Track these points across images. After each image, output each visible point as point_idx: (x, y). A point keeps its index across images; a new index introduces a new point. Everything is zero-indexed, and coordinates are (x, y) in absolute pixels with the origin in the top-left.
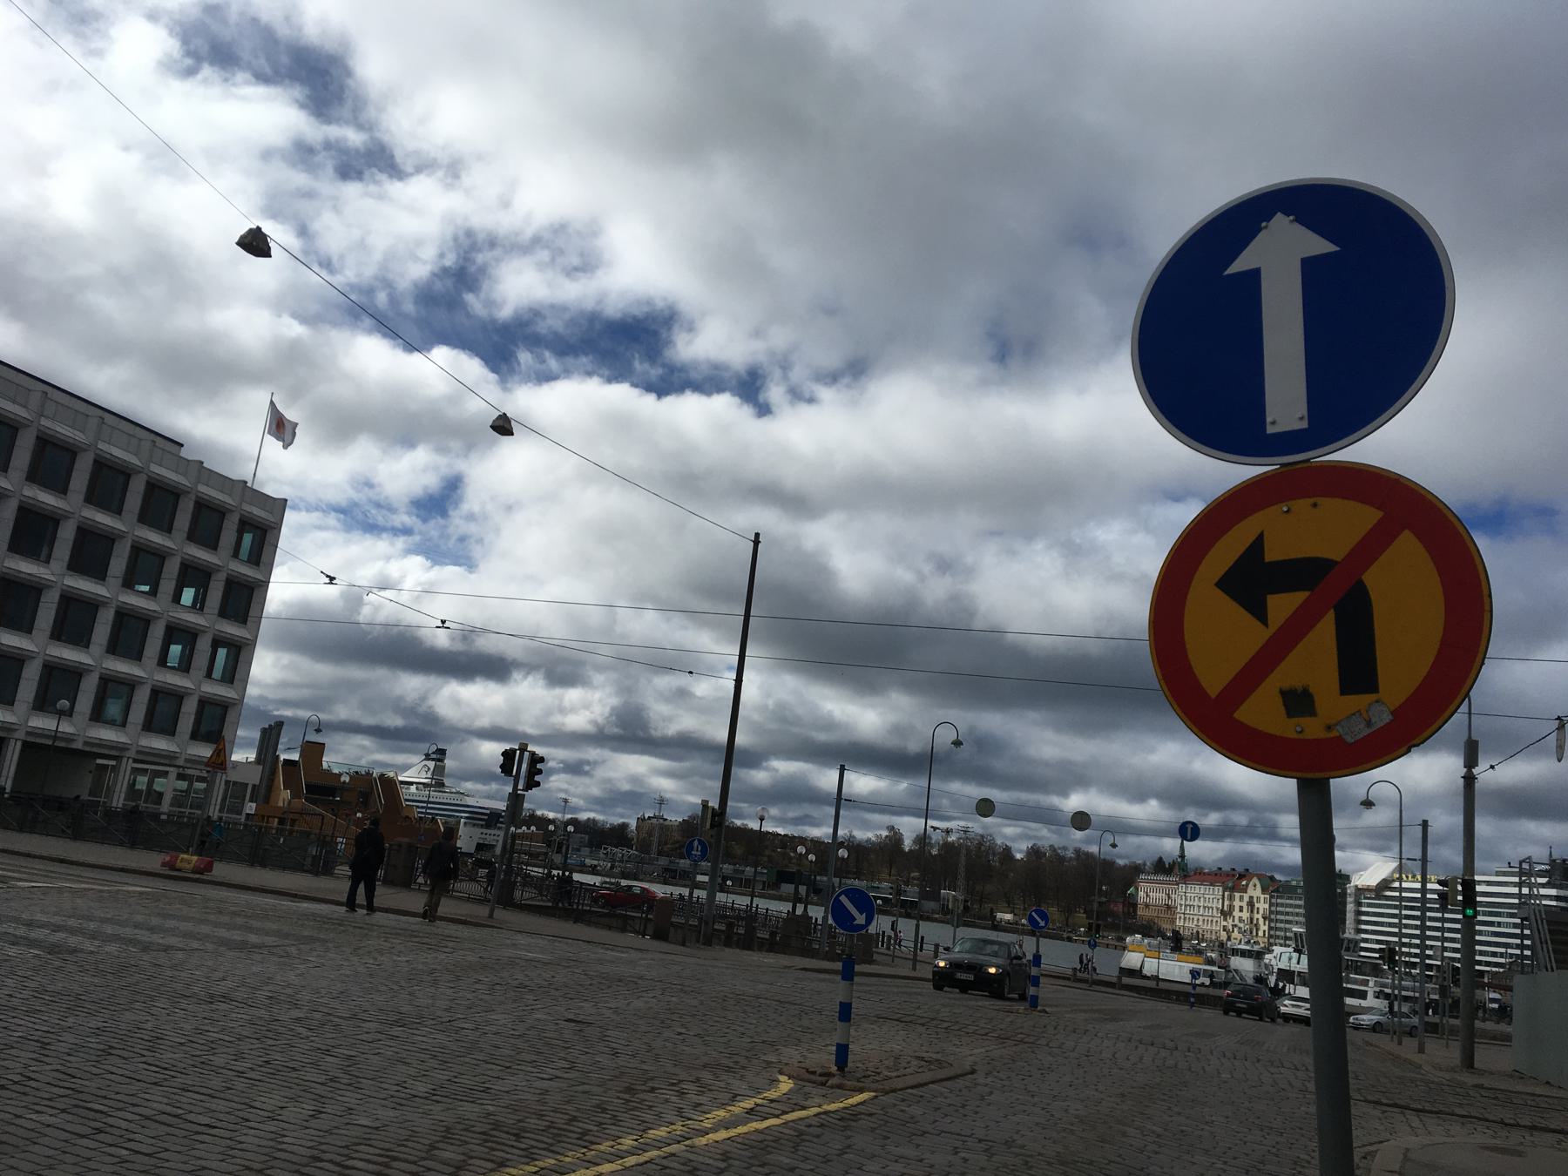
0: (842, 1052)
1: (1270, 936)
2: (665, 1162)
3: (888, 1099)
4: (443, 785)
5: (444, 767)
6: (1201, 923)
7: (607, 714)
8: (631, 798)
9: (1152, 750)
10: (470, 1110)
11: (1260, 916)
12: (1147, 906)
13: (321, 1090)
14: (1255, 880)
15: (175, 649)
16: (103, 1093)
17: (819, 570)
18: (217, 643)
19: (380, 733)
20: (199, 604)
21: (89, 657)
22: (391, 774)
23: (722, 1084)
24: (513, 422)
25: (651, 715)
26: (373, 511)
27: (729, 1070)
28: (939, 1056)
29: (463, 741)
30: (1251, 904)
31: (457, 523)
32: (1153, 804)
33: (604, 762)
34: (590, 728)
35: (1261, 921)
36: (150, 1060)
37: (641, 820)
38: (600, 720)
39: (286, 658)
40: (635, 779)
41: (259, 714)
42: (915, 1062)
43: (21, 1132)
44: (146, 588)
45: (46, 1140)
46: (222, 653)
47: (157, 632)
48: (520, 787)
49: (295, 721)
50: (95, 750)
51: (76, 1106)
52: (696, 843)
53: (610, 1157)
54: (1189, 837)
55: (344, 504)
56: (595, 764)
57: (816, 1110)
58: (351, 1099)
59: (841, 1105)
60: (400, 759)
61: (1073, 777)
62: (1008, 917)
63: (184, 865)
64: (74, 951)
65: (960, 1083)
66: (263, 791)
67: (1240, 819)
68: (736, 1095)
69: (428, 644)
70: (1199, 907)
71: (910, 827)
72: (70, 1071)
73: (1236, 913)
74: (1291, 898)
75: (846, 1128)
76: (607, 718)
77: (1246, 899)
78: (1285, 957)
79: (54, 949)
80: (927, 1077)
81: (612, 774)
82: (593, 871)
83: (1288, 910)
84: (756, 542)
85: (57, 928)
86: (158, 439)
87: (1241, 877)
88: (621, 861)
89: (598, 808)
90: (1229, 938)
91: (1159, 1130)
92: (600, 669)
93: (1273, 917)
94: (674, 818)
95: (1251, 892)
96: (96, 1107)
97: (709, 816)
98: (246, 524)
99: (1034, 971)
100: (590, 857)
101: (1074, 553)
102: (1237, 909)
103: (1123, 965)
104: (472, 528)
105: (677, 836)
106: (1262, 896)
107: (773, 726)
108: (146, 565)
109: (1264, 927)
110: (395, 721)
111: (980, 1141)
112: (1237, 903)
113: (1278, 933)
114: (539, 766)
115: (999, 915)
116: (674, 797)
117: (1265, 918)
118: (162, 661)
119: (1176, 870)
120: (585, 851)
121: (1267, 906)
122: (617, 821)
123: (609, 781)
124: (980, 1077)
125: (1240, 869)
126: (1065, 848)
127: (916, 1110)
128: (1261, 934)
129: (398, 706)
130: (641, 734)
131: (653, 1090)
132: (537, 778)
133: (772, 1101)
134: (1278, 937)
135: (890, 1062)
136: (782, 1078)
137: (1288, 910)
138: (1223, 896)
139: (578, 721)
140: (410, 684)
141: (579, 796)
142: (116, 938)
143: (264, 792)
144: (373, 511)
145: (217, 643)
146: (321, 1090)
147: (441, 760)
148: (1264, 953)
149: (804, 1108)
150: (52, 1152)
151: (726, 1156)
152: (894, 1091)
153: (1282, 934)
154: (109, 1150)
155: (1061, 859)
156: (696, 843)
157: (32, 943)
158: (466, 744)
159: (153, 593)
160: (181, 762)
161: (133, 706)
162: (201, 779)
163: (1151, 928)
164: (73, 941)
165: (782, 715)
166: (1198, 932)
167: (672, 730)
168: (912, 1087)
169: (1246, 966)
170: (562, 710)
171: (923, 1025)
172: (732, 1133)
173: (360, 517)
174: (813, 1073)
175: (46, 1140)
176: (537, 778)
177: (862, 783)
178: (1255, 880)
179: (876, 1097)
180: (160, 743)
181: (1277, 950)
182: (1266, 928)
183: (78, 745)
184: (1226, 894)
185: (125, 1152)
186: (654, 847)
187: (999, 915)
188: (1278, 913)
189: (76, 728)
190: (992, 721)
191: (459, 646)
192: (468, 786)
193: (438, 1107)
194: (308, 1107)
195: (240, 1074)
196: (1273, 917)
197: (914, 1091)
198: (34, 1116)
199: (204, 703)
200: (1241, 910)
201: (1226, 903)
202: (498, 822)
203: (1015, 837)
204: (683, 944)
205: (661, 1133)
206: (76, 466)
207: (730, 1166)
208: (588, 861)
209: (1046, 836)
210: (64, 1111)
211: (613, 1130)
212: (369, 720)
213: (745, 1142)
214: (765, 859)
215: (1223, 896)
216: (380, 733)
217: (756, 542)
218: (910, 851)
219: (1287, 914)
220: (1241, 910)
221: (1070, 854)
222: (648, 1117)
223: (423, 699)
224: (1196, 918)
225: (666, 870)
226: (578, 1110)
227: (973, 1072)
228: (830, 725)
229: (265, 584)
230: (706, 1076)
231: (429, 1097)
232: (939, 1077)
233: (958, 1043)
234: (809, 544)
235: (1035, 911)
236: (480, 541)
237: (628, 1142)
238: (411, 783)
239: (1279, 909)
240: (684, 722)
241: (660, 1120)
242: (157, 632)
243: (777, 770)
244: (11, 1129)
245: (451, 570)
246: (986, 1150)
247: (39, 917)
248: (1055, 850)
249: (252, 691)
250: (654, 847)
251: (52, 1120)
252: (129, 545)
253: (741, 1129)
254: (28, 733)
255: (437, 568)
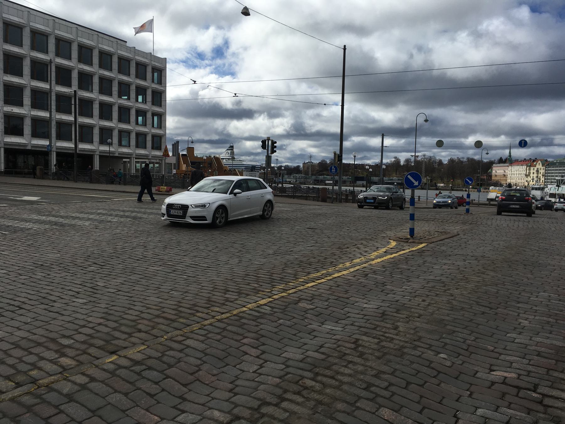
0: (412, 231)
1: (545, 182)
2: (363, 270)
3: (432, 245)
4: (234, 158)
5: (233, 152)
6: (517, 180)
7: (290, 126)
8: (301, 156)
9: (504, 116)
10: (291, 258)
11: (541, 175)
12: (496, 176)
13: (238, 254)
14: (539, 162)
15: (140, 119)
16: (170, 260)
17: (369, 58)
18: (153, 115)
19: (211, 142)
20: (144, 101)
21: (113, 124)
22: (218, 156)
23: (371, 244)
24: (249, 10)
25: (306, 125)
26: (195, 60)
27: (371, 240)
28: (444, 230)
29: (239, 142)
30: (537, 171)
31: (229, 59)
32: (503, 138)
33: (290, 144)
34: (284, 133)
35: (541, 177)
36: (180, 249)
37: (304, 164)
38: (288, 129)
39: (176, 119)
40: (302, 150)
41: (171, 139)
42: (436, 233)
43: (150, 273)
44: (126, 97)
45: (159, 275)
46: (156, 118)
47: (133, 112)
48: (269, 153)
49: (184, 141)
50: (122, 156)
51: (164, 264)
52: (333, 167)
53: (344, 269)
54: (523, 146)
55: (184, 59)
56: (287, 145)
57: (408, 251)
58: (249, 256)
59: (416, 248)
60: (219, 150)
61: (470, 130)
62: (442, 185)
63: (163, 190)
64: (141, 218)
65: (455, 239)
66: (177, 165)
67: (537, 139)
68: (378, 247)
69: (224, 108)
70: (517, 174)
71: (403, 157)
72: (156, 254)
73: (532, 175)
74: (554, 167)
75: (421, 255)
76: (290, 128)
77: (536, 169)
78: (553, 189)
79: (135, 218)
80: (443, 237)
81: (293, 149)
82: (290, 183)
83: (552, 172)
84: (345, 49)
85: (132, 212)
86: (119, 42)
87: (534, 161)
88: (299, 179)
89: (290, 161)
90: (528, 184)
91: (537, 249)
92: (287, 109)
93: (546, 175)
94: (316, 162)
95: (538, 166)
96: (170, 264)
97: (337, 157)
98: (154, 69)
99: (468, 200)
100: (288, 178)
101: (477, 36)
102: (532, 173)
103: (489, 197)
104: (232, 60)
105: (317, 168)
106: (542, 168)
107: (352, 124)
108: (124, 89)
109: (542, 179)
110: (215, 137)
111: (472, 256)
112: (532, 171)
113: (548, 181)
114: (275, 145)
115: (439, 185)
116: (316, 154)
117: (543, 176)
118: (137, 123)
119: (509, 161)
120: (286, 176)
121: (544, 171)
122: (296, 165)
123: (293, 151)
124: (462, 236)
125: (533, 158)
126: (463, 158)
127: (443, 248)
128: (541, 181)
129: (216, 132)
130: (302, 132)
131: (348, 248)
132: (275, 149)
133: (391, 248)
134: (548, 182)
135: (427, 233)
136: (391, 241)
137: (552, 172)
138: (526, 169)
139: (279, 130)
140: (219, 124)
141: (282, 158)
142: (152, 213)
143: (178, 166)
144: (195, 60)
145: (153, 115)
146: (238, 254)
147: (232, 150)
148: (545, 188)
149: (404, 250)
150: (162, 278)
151: (384, 267)
152: (433, 242)
153: (550, 181)
154: (180, 276)
155: (462, 162)
156: (333, 167)
157: (127, 217)
158: (240, 143)
159: (129, 99)
160: (150, 157)
161: (131, 140)
162: (157, 163)
163: (497, 184)
164: (139, 215)
165: (355, 120)
166: (516, 183)
167: (314, 130)
168: (439, 241)
169: (538, 194)
170: (273, 127)
171: (433, 221)
172: (382, 259)
173: (191, 63)
174: (402, 239)
175: (159, 275)
176: (275, 149)
177: (388, 142)
178: (539, 162)
179: (428, 245)
180: (142, 152)
181: (549, 186)
182: (543, 179)
183: (117, 155)
184: (528, 168)
185: (185, 277)
186: (310, 173)
187: (439, 185)
188: (548, 173)
189: (114, 149)
190: (437, 112)
191: (236, 107)
192: (243, 158)
193: (278, 257)
194: (237, 260)
195: (210, 251)
196: (546, 175)
197: (440, 242)
198: (152, 268)
199: (154, 136)
200: (533, 173)
201: (528, 171)
202: (255, 169)
203: (444, 156)
204: (332, 203)
205: (358, 260)
206: (93, 54)
207: (386, 270)
208: (288, 180)
209: (457, 154)
210: (160, 266)
211: (341, 261)
212: (207, 138)
213: (390, 262)
214: (350, 173)
215: (526, 169)
216: (211, 142)
217: (345, 49)
218: (403, 165)
219: (552, 173)
220: (533, 173)
221: (465, 160)
222: (352, 256)
223: (225, 128)
224: (515, 178)
225: (315, 180)
226: (326, 255)
227: (458, 235)
228: (374, 121)
229: (164, 92)
230: (364, 242)
231: (274, 254)
232: (447, 237)
233: (385, 235)
234: (366, 48)
235: (467, 178)
236: (237, 64)
237: (348, 264)
238: (224, 159)
239: (549, 175)
240: (319, 126)
241: (355, 257)
242: (133, 112)
243: (354, 141)
244: (146, 272)
245: (228, 78)
246: (476, 259)
247: (125, 209)
248: (459, 159)
249: (167, 132)
250: (310, 173)
251: (158, 269)
252: (117, 82)
253: (385, 258)
254: (100, 152)
255: (221, 78)
